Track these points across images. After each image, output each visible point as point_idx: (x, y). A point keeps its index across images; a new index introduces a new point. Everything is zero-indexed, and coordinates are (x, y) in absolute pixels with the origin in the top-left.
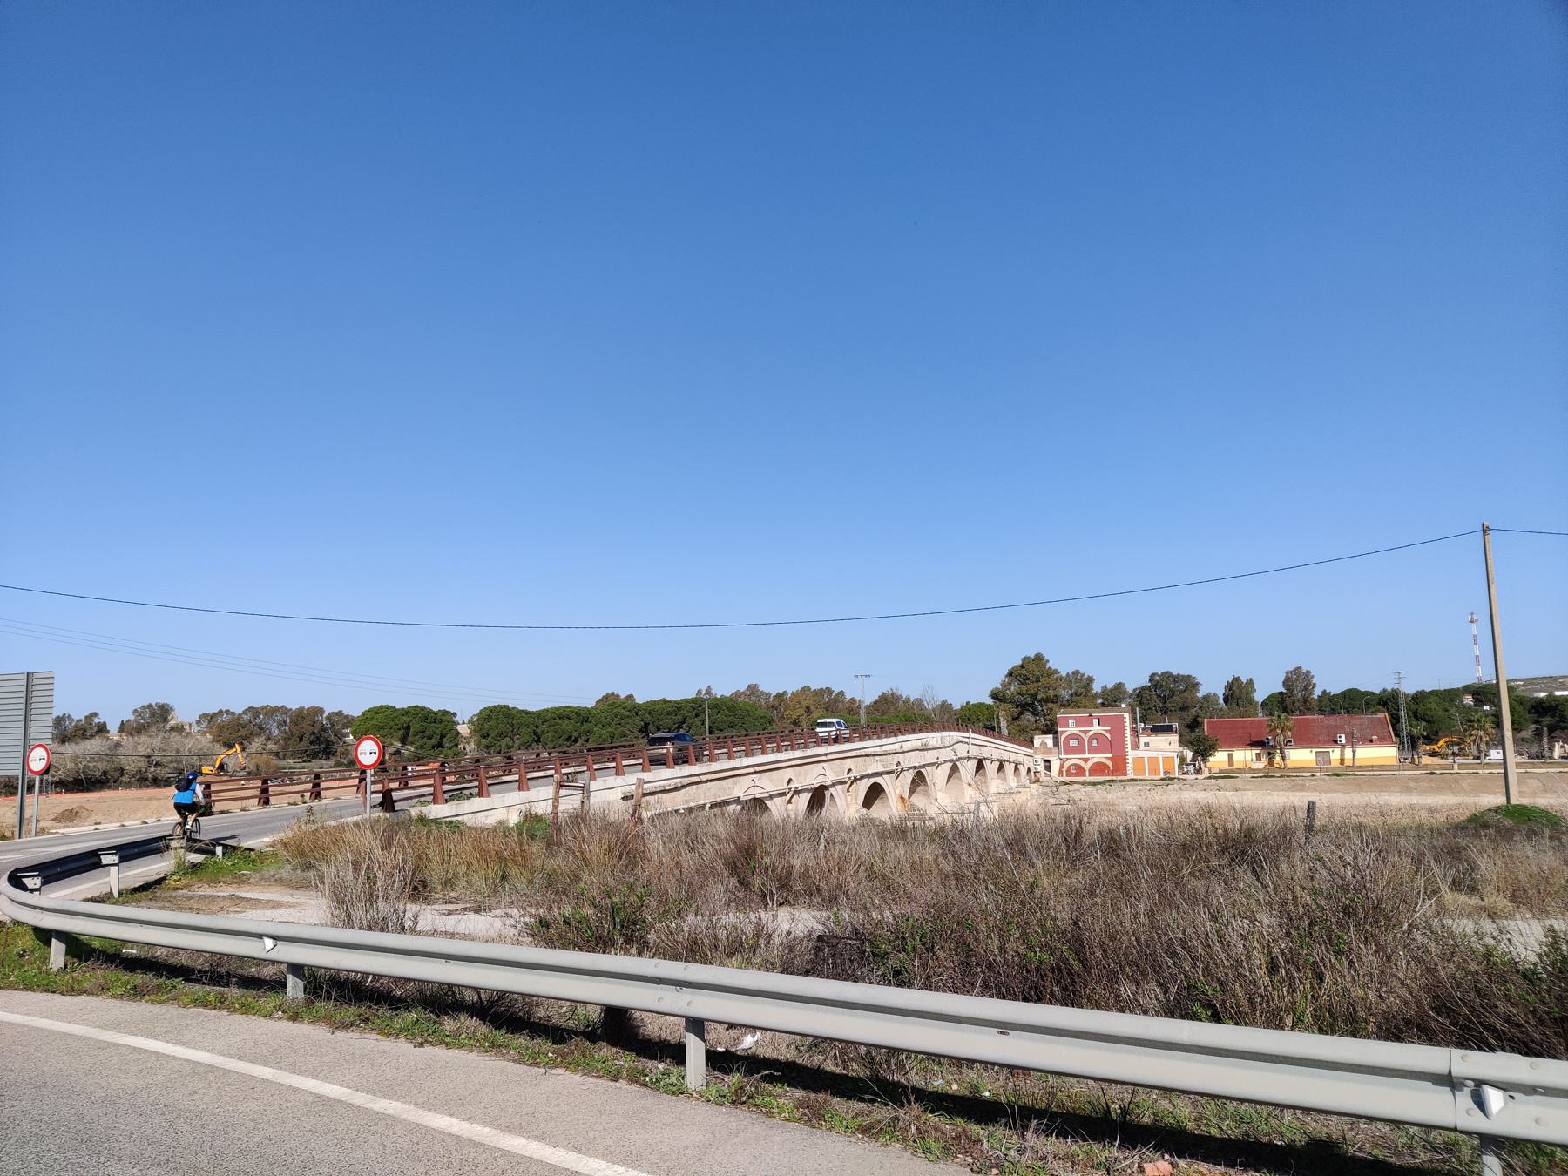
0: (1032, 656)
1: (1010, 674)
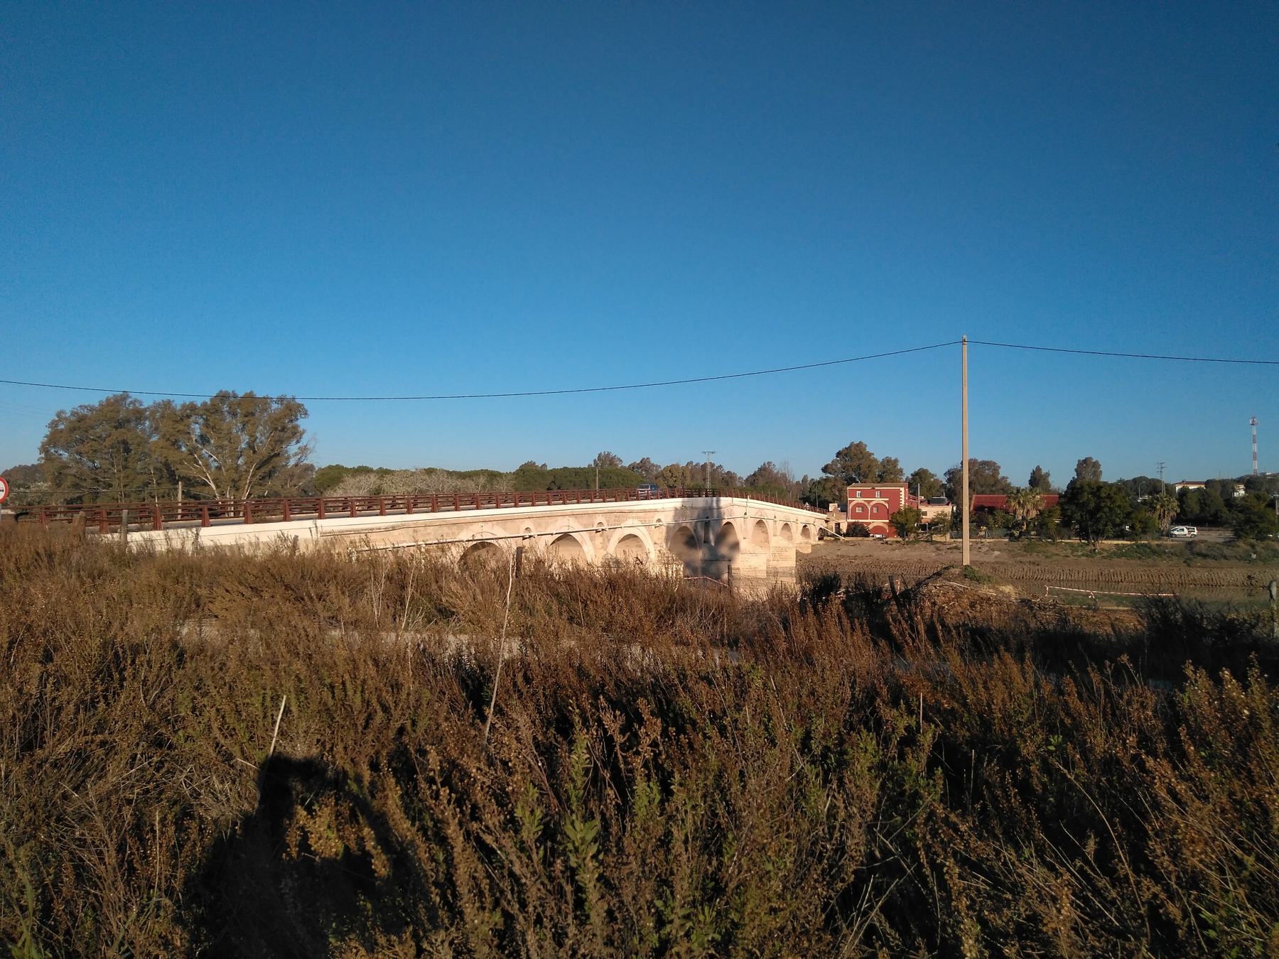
0: (241, 394)
1: (839, 454)
